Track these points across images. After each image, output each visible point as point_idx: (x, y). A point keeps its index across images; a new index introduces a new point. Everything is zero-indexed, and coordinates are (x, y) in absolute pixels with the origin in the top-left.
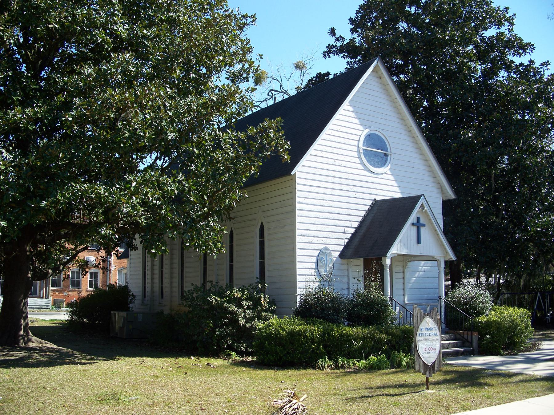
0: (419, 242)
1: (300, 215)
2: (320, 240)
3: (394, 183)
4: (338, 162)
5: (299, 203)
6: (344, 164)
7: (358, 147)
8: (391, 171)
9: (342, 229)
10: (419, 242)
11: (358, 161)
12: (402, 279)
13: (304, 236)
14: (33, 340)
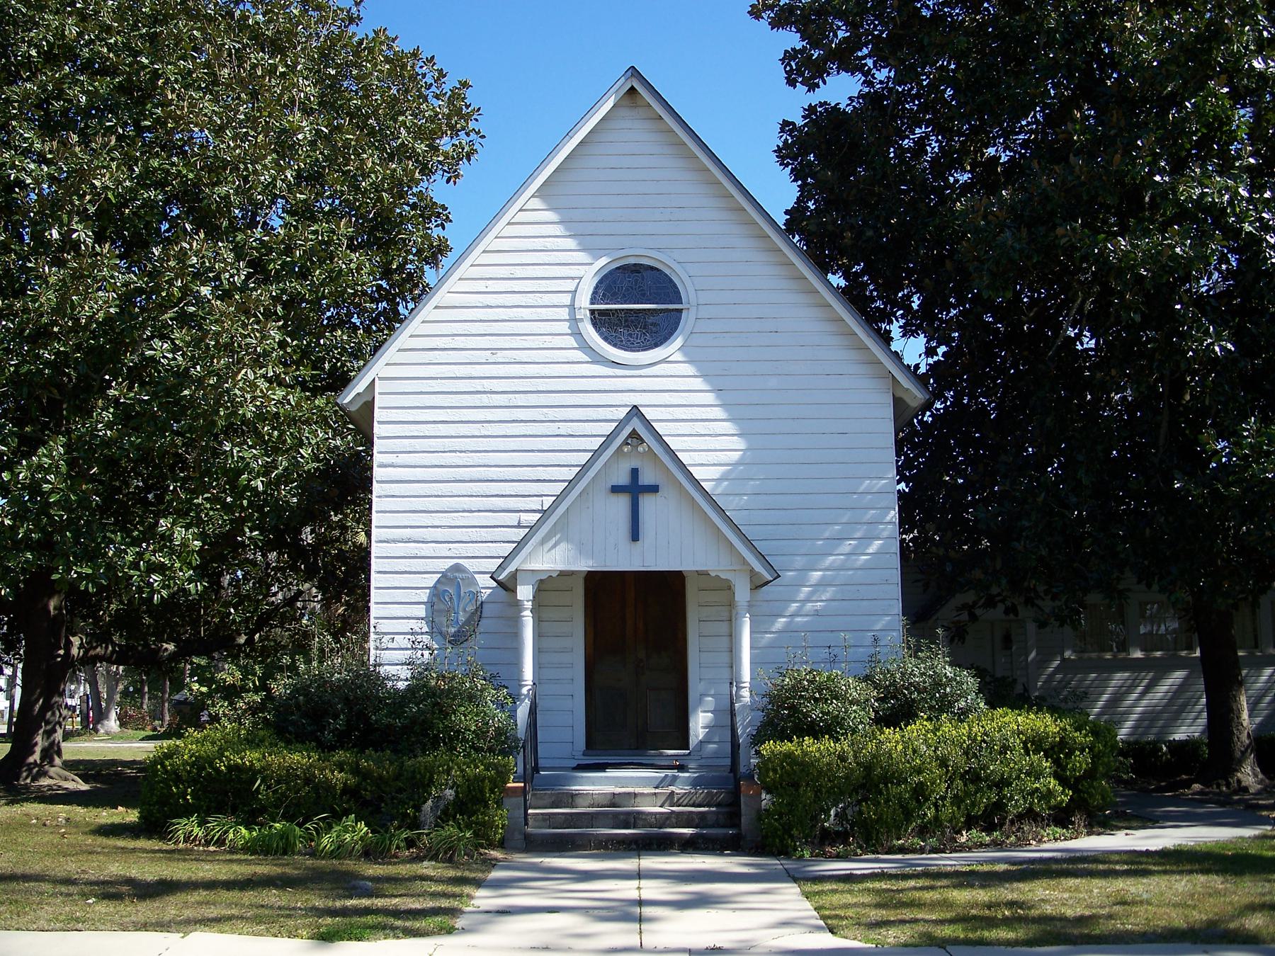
0: (635, 536)
1: (383, 493)
2: (443, 549)
3: (698, 383)
4: (500, 356)
5: (381, 466)
6: (523, 356)
7: (572, 307)
8: (685, 354)
9: (512, 519)
10: (635, 536)
11: (571, 342)
12: (726, 639)
13: (394, 541)
14: (51, 773)
